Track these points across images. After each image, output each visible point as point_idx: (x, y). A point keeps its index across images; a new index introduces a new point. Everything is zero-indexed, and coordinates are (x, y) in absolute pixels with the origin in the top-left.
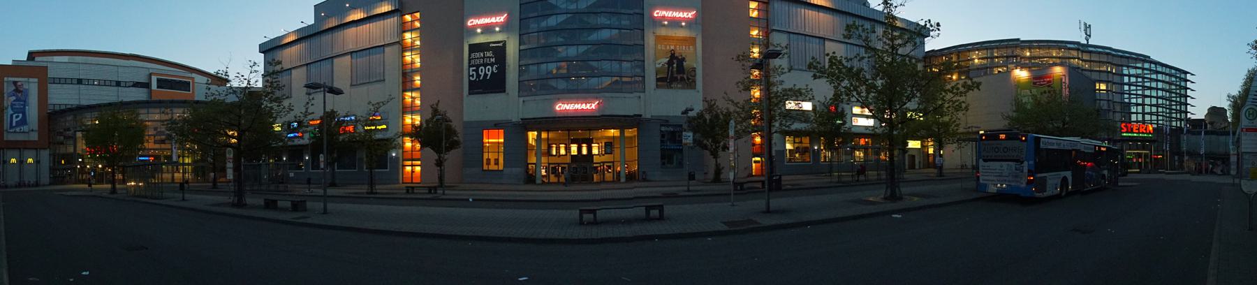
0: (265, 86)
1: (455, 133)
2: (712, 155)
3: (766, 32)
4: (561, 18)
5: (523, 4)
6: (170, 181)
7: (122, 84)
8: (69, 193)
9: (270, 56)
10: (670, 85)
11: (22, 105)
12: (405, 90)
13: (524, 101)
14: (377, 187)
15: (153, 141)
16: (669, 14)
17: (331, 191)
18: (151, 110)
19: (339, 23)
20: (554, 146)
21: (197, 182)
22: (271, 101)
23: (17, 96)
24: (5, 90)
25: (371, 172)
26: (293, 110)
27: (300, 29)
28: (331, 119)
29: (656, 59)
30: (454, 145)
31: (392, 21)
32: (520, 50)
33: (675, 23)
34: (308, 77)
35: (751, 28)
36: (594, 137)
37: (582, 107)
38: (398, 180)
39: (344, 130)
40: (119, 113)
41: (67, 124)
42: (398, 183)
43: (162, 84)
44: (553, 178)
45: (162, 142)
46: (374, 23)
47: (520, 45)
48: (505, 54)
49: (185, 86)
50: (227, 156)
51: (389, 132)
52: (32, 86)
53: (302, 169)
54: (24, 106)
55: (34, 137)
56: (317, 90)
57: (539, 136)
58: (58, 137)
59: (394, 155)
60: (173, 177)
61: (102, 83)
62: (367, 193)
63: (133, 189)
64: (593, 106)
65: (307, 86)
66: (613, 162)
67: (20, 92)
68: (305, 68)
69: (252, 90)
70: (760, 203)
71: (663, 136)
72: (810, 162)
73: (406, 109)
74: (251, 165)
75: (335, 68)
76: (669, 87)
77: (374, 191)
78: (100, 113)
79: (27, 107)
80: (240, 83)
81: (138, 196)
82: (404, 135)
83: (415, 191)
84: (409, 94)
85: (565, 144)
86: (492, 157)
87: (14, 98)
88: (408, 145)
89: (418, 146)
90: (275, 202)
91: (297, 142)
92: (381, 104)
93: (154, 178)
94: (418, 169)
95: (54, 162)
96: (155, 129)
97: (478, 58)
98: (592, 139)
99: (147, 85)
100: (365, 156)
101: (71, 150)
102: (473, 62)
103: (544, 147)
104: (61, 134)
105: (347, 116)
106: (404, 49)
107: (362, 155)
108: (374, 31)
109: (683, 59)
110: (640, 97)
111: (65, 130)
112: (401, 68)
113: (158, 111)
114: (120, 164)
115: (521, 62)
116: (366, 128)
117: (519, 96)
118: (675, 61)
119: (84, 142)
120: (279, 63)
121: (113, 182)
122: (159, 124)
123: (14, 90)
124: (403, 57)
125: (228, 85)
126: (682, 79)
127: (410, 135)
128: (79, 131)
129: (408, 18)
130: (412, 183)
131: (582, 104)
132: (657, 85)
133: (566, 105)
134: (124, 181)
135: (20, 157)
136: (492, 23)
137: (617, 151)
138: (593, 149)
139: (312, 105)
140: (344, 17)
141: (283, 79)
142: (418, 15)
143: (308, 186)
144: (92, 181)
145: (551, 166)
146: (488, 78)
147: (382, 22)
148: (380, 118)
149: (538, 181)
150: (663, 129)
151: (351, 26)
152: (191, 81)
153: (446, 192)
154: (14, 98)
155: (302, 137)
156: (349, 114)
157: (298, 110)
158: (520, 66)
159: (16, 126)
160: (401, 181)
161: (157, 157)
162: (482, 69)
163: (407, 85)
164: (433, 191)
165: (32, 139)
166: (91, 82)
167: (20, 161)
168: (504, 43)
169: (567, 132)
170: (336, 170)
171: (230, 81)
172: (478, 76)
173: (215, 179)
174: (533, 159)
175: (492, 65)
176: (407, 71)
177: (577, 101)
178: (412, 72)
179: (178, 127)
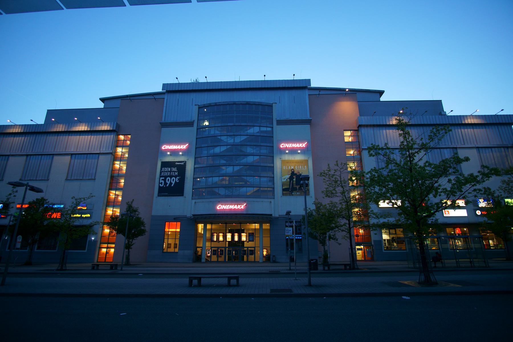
1: (143, 224)
2: (321, 243)
3: (359, 151)
4: (223, 149)
10: (291, 193)
12: (111, 189)
13: (195, 203)
14: (67, 265)
16: (290, 145)
19: (66, 130)
20: (215, 234)
27: (25, 125)
30: (142, 233)
31: (110, 137)
32: (194, 168)
33: (293, 151)
35: (347, 149)
36: (245, 228)
37: (235, 208)
44: (214, 258)
46: (95, 136)
47: (195, 165)
57: (205, 227)
62: (57, 270)
64: (242, 207)
66: (254, 247)
68: (25, 157)
70: (305, 280)
72: (406, 250)
75: (53, 164)
76: (291, 194)
85: (223, 233)
88: (107, 231)
94: (112, 250)
97: (166, 172)
98: (244, 230)
102: (163, 174)
103: (208, 235)
106: (115, 158)
108: (94, 143)
110: (271, 202)
112: (110, 173)
124: (114, 164)
127: (108, 224)
129: (122, 137)
132: (283, 193)
136: (178, 149)
137: (257, 239)
140: (71, 127)
142: (130, 136)
145: (213, 249)
146: (172, 185)
147: (101, 136)
149: (203, 260)
162: (168, 179)
163: (113, 184)
168: (185, 163)
169: (225, 224)
170: (36, 250)
172: (166, 183)
174: (200, 244)
175: (176, 177)
176: (115, 175)
177: (231, 203)
178: (118, 176)
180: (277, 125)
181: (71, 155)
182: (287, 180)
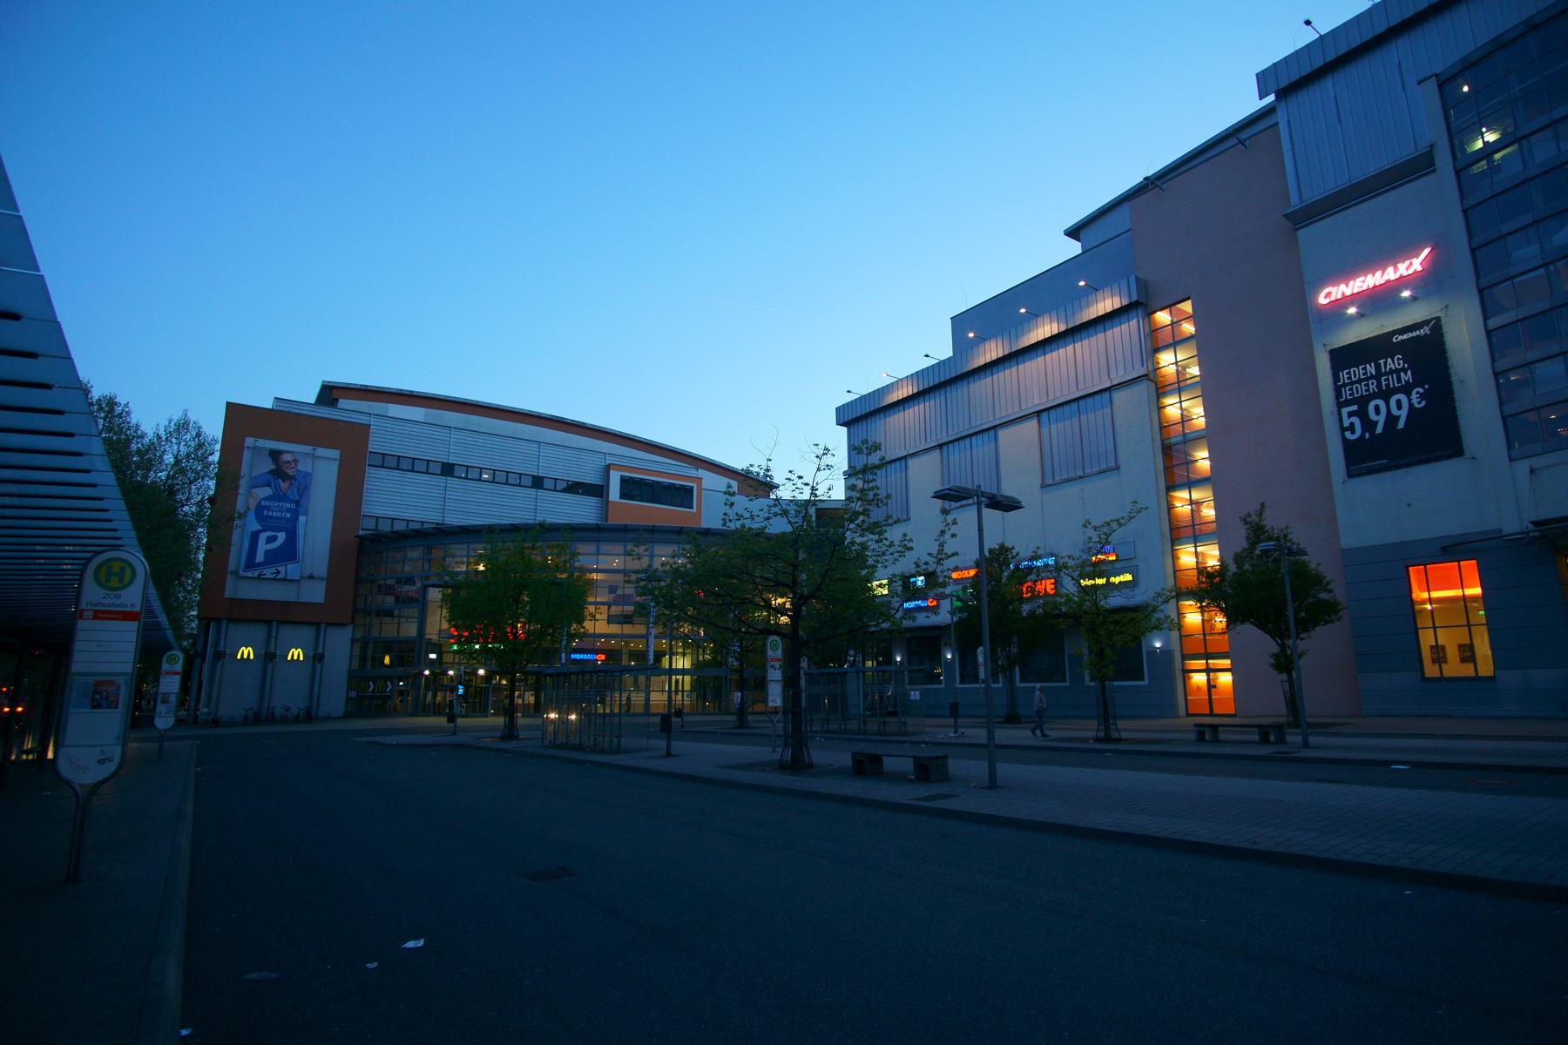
0: (848, 499)
1: (1319, 581)
6: (640, 710)
7: (547, 484)
8: (394, 740)
9: (860, 429)
11: (289, 510)
12: (1171, 487)
13: (1532, 471)
15: (605, 616)
17: (1005, 735)
18: (604, 547)
21: (704, 714)
22: (864, 530)
23: (277, 488)
24: (244, 469)
25: (1103, 687)
26: (911, 549)
28: (1000, 566)
30: (1323, 613)
31: (1129, 329)
34: (945, 472)
38: (1174, 705)
39: (1032, 589)
40: (533, 548)
41: (407, 569)
42: (1177, 716)
43: (632, 488)
45: (626, 619)
46: (1086, 342)
47: (1486, 318)
49: (682, 495)
50: (770, 653)
51: (1137, 591)
52: (323, 468)
53: (940, 682)
54: (295, 515)
55: (315, 593)
56: (964, 502)
58: (380, 598)
59: (1158, 645)
60: (647, 700)
61: (500, 477)
62: (1097, 740)
63: (551, 728)
65: (939, 495)
67: (286, 477)
68: (936, 453)
69: (821, 506)
73: (1180, 532)
74: (822, 674)
77: (1115, 735)
78: (489, 546)
79: (302, 518)
80: (794, 494)
81: (562, 747)
82: (1180, 594)
84: (1183, 494)
86: (1450, 640)
87: (267, 491)
88: (1193, 618)
89: (1220, 621)
90: (877, 759)
91: (922, 620)
92: (1114, 525)
93: (603, 702)
94: (1225, 679)
95: (363, 659)
96: (612, 589)
97: (1359, 381)
99: (598, 491)
100: (1085, 651)
101: (411, 630)
102: (1346, 393)
104: (389, 590)
105: (1036, 558)
107: (1079, 647)
111: (399, 581)
112: (1158, 437)
113: (619, 548)
114: (534, 666)
116: (1083, 583)
117: (1511, 460)
119: (445, 612)
120: (877, 447)
121: (510, 711)
122: (620, 577)
123: (272, 472)
124: (1161, 408)
125: (773, 496)
127: (1197, 595)
128: (433, 586)
129: (1163, 317)
130: (1211, 714)
134: (538, 709)
135: (268, 642)
139: (953, 536)
141: (886, 482)
142: (1187, 307)
143: (952, 720)
144: (457, 709)
146: (1401, 425)
148: (1113, 558)
152: (695, 485)
153: (1312, 740)
154: (267, 491)
155: (934, 610)
156: (1039, 552)
157: (923, 548)
158: (1496, 375)
159: (265, 564)
160: (1182, 710)
161: (612, 654)
163: (1175, 472)
164: (1272, 738)
165: (305, 598)
166: (473, 474)
167: (314, 657)
168: (1436, 326)
171: (777, 487)
172: (1368, 425)
173: (742, 703)
175: (1406, 389)
179: (661, 588)
181: (1038, 416)
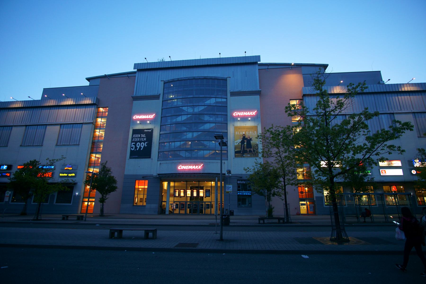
5: (164, 101)
10: (243, 155)
12: (92, 152)
13: (160, 164)
16: (241, 114)
20: (177, 191)
29: (234, 140)
31: (91, 110)
33: (244, 119)
46: (80, 109)
47: (160, 131)
48: (152, 136)
62: (34, 220)
64: (200, 167)
68: (24, 127)
71: (239, 187)
75: (47, 132)
76: (242, 156)
83: (69, 219)
97: (137, 138)
103: (172, 191)
106: (96, 127)
108: (79, 115)
109: (251, 139)
115: (161, 132)
118: (245, 141)
124: (95, 132)
126: (250, 151)
129: (101, 109)
131: (193, 166)
133: (184, 166)
136: (147, 118)
138: (200, 193)
146: (142, 149)
147: (84, 109)
148: (71, 169)
149: (167, 213)
150: (239, 182)
151: (64, 108)
162: (138, 144)
168: (152, 130)
169: (185, 182)
172: (136, 148)
175: (144, 142)
176: (96, 141)
178: (98, 142)
180: (231, 96)
182: (239, 143)
